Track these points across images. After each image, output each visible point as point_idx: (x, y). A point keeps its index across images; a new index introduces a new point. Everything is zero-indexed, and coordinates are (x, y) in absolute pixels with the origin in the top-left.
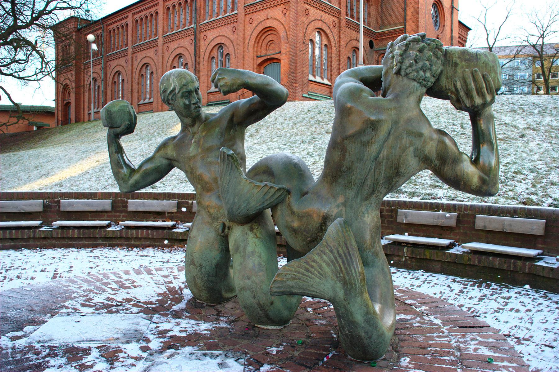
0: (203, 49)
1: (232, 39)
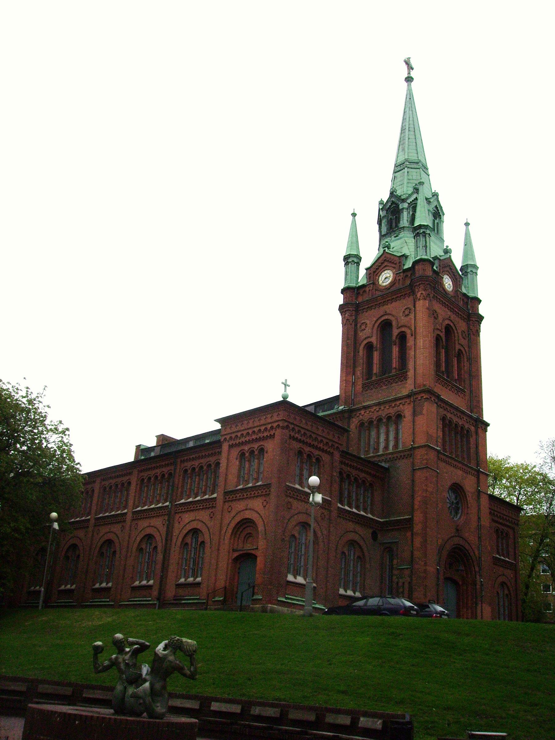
0: (176, 532)
1: (209, 525)
